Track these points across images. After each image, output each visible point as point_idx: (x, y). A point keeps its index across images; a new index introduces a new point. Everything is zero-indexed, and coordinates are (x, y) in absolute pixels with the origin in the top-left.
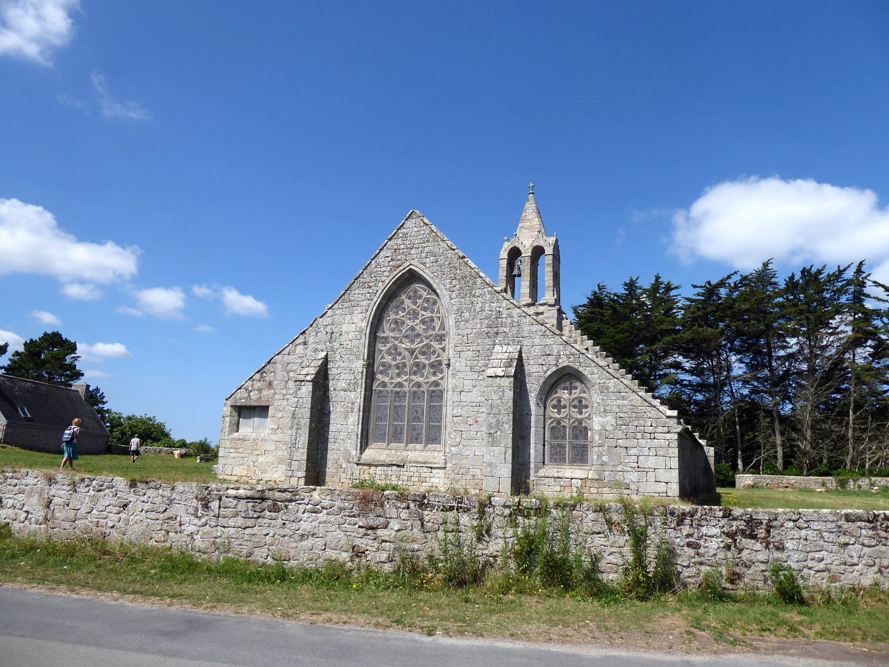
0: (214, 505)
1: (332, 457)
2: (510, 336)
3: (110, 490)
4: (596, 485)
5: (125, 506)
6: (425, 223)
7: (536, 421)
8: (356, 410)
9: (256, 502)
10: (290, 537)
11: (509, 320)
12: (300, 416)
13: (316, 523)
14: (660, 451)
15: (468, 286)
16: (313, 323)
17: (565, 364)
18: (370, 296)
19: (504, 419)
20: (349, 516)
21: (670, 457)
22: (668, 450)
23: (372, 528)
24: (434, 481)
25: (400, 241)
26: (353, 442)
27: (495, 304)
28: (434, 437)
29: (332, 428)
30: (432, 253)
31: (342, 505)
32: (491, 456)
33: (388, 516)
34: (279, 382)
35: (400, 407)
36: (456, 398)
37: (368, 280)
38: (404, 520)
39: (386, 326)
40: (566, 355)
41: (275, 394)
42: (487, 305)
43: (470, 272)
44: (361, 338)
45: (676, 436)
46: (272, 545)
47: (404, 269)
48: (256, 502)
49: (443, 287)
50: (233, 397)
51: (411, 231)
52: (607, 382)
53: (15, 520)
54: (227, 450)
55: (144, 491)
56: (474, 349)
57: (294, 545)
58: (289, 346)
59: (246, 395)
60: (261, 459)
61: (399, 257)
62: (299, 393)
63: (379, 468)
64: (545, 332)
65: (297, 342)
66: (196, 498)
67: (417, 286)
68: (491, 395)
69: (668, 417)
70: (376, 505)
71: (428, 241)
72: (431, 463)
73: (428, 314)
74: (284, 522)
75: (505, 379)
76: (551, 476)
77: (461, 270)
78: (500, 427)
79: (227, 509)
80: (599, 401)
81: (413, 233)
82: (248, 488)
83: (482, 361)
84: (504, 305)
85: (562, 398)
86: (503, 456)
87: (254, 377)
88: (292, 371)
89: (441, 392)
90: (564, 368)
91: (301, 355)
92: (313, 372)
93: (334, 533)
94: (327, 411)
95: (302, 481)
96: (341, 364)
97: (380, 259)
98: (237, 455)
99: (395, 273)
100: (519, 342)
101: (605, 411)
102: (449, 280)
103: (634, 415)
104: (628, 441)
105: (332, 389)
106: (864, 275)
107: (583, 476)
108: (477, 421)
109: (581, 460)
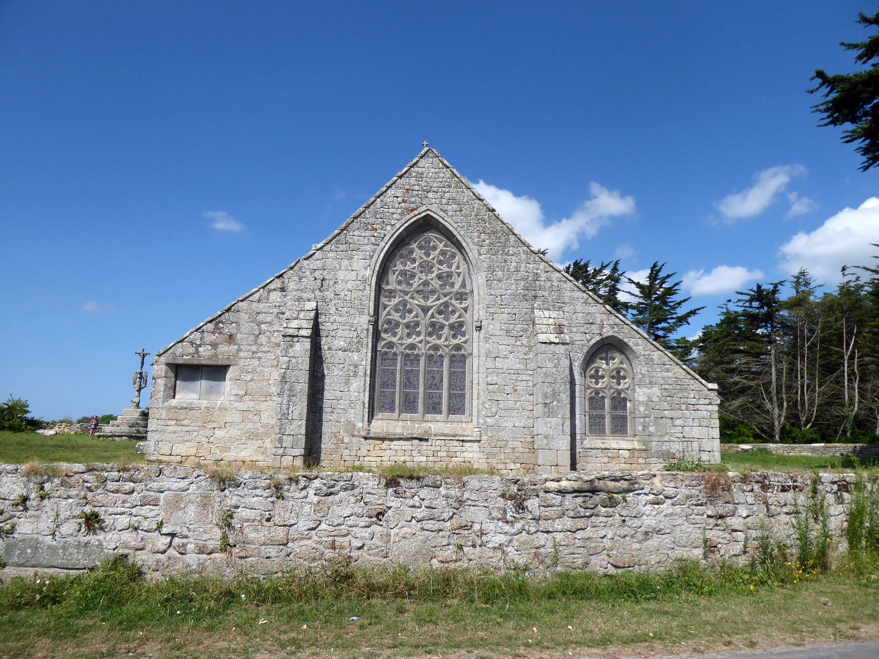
0: (532, 504)
1: (330, 430)
2: (549, 300)
3: (351, 492)
4: (644, 455)
5: (380, 515)
6: (445, 165)
7: (581, 391)
8: (361, 373)
9: (587, 496)
10: (632, 537)
11: (548, 284)
12: (293, 379)
13: (660, 517)
14: (703, 421)
15: (500, 243)
16: (295, 266)
17: (610, 334)
18: (376, 240)
19: (561, 389)
20: (696, 505)
21: (712, 428)
22: (710, 421)
23: (722, 517)
24: (466, 456)
25: (413, 181)
26: (358, 412)
27: (531, 266)
28: (457, 406)
29: (327, 395)
30: (455, 200)
31: (688, 492)
32: (547, 427)
33: (736, 502)
34: (246, 336)
35: (411, 372)
36: (490, 364)
37: (372, 220)
38: (750, 504)
39: (392, 278)
40: (610, 325)
41: (239, 350)
42: (523, 265)
43: (502, 227)
44: (364, 289)
45: (717, 408)
46: (612, 550)
47: (420, 214)
48: (587, 496)
49: (469, 240)
50: (169, 352)
51: (427, 172)
52: (652, 354)
53: (142, 549)
54: (162, 422)
55: (412, 490)
56: (510, 312)
57: (638, 546)
58: (259, 291)
59: (192, 350)
60: (219, 433)
61: (413, 199)
62: (290, 350)
63: (395, 443)
64: (587, 299)
65: (271, 287)
66: (503, 496)
67: (431, 235)
68: (546, 362)
69: (710, 390)
70: (723, 489)
71: (450, 186)
72: (462, 436)
73: (445, 268)
74: (623, 518)
75: (561, 346)
76: (598, 447)
77: (490, 223)
78: (556, 397)
79: (549, 509)
80: (644, 373)
81: (431, 174)
82: (574, 479)
83: (519, 326)
84: (541, 267)
85: (601, 368)
86: (561, 427)
87: (204, 328)
88: (265, 323)
89: (463, 356)
90: (608, 337)
91: (277, 304)
92: (306, 326)
93: (683, 526)
94: (320, 375)
95: (299, 462)
96: (337, 318)
97: (388, 198)
98: (179, 428)
99: (408, 217)
100: (560, 308)
101: (650, 383)
102: (476, 234)
103: (678, 387)
104: (673, 412)
105: (326, 347)
106: (619, 272)
107: (631, 447)
108: (516, 390)
109: (620, 431)
